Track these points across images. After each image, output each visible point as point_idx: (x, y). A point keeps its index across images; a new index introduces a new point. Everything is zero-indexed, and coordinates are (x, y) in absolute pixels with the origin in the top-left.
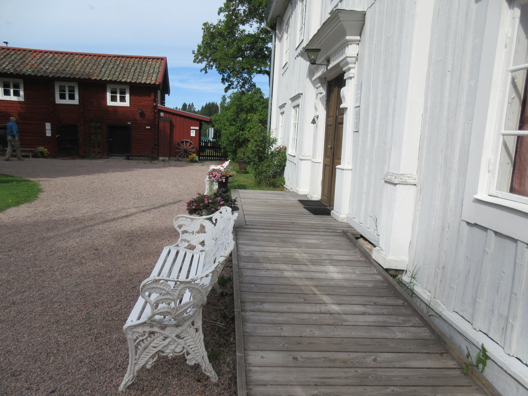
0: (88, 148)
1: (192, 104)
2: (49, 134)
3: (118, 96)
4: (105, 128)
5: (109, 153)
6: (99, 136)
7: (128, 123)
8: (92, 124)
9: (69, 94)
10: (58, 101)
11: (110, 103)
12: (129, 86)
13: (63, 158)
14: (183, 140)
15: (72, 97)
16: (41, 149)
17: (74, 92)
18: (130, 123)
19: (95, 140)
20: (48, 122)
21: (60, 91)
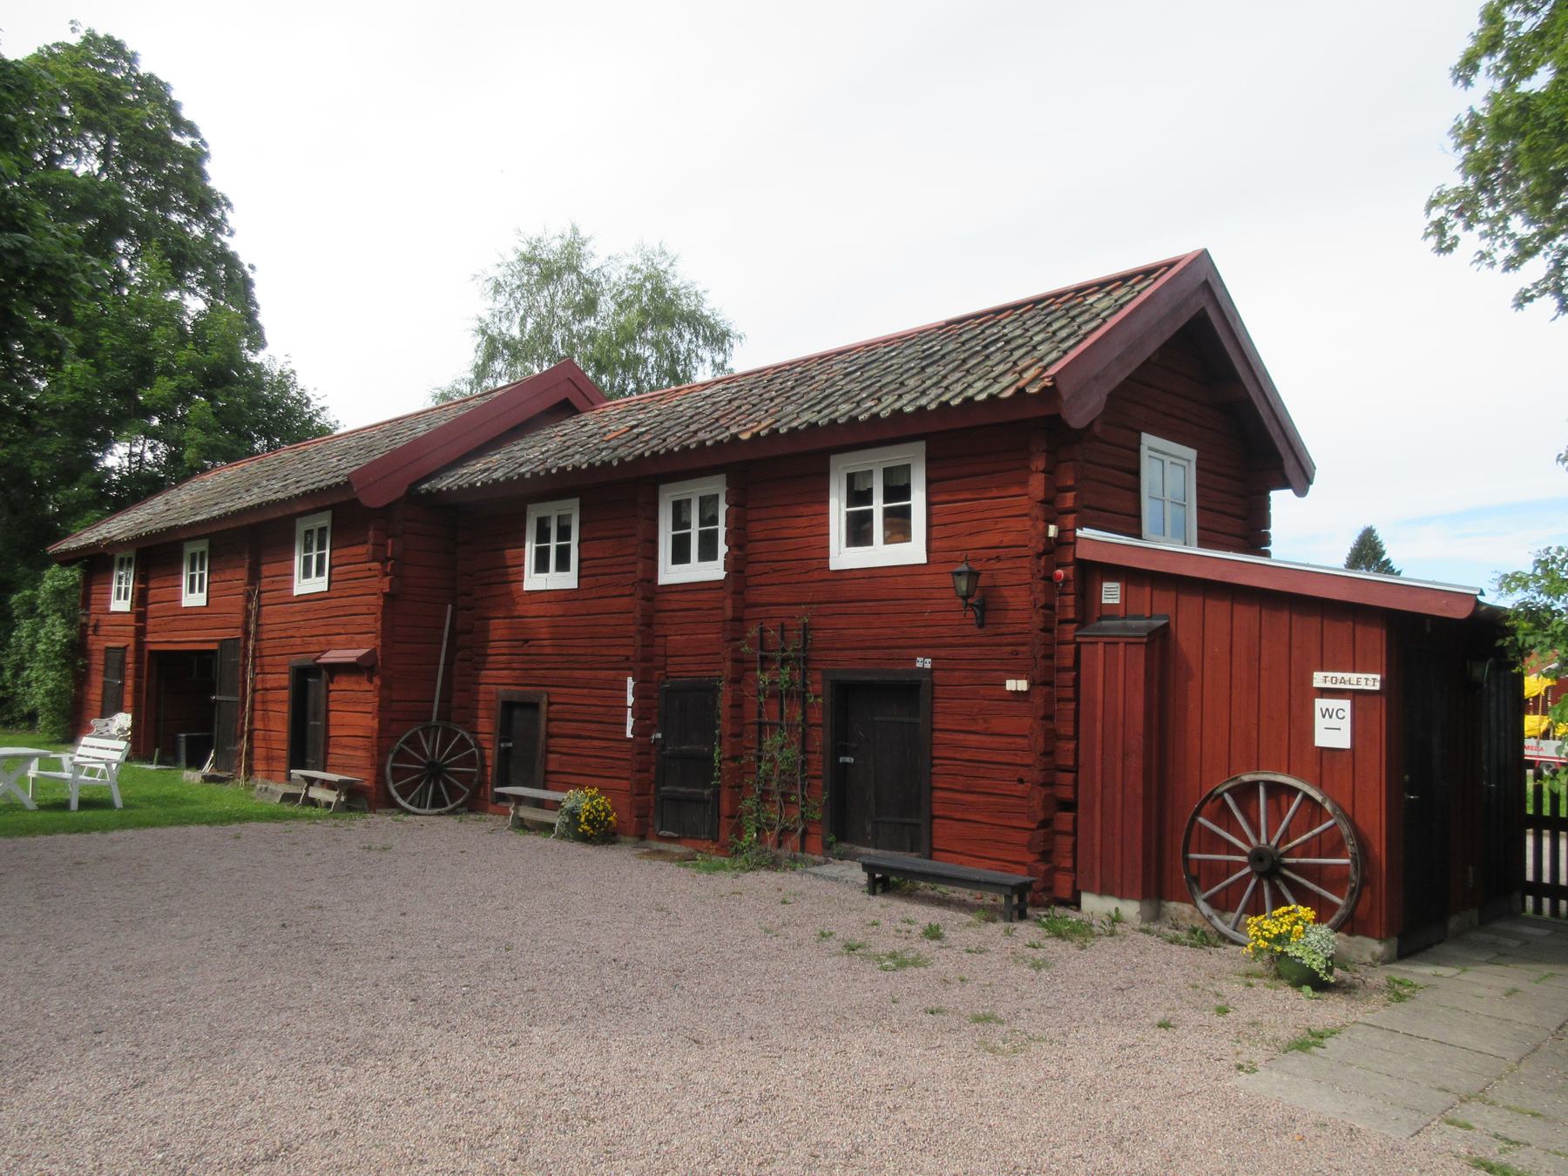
14: (1246, 778)
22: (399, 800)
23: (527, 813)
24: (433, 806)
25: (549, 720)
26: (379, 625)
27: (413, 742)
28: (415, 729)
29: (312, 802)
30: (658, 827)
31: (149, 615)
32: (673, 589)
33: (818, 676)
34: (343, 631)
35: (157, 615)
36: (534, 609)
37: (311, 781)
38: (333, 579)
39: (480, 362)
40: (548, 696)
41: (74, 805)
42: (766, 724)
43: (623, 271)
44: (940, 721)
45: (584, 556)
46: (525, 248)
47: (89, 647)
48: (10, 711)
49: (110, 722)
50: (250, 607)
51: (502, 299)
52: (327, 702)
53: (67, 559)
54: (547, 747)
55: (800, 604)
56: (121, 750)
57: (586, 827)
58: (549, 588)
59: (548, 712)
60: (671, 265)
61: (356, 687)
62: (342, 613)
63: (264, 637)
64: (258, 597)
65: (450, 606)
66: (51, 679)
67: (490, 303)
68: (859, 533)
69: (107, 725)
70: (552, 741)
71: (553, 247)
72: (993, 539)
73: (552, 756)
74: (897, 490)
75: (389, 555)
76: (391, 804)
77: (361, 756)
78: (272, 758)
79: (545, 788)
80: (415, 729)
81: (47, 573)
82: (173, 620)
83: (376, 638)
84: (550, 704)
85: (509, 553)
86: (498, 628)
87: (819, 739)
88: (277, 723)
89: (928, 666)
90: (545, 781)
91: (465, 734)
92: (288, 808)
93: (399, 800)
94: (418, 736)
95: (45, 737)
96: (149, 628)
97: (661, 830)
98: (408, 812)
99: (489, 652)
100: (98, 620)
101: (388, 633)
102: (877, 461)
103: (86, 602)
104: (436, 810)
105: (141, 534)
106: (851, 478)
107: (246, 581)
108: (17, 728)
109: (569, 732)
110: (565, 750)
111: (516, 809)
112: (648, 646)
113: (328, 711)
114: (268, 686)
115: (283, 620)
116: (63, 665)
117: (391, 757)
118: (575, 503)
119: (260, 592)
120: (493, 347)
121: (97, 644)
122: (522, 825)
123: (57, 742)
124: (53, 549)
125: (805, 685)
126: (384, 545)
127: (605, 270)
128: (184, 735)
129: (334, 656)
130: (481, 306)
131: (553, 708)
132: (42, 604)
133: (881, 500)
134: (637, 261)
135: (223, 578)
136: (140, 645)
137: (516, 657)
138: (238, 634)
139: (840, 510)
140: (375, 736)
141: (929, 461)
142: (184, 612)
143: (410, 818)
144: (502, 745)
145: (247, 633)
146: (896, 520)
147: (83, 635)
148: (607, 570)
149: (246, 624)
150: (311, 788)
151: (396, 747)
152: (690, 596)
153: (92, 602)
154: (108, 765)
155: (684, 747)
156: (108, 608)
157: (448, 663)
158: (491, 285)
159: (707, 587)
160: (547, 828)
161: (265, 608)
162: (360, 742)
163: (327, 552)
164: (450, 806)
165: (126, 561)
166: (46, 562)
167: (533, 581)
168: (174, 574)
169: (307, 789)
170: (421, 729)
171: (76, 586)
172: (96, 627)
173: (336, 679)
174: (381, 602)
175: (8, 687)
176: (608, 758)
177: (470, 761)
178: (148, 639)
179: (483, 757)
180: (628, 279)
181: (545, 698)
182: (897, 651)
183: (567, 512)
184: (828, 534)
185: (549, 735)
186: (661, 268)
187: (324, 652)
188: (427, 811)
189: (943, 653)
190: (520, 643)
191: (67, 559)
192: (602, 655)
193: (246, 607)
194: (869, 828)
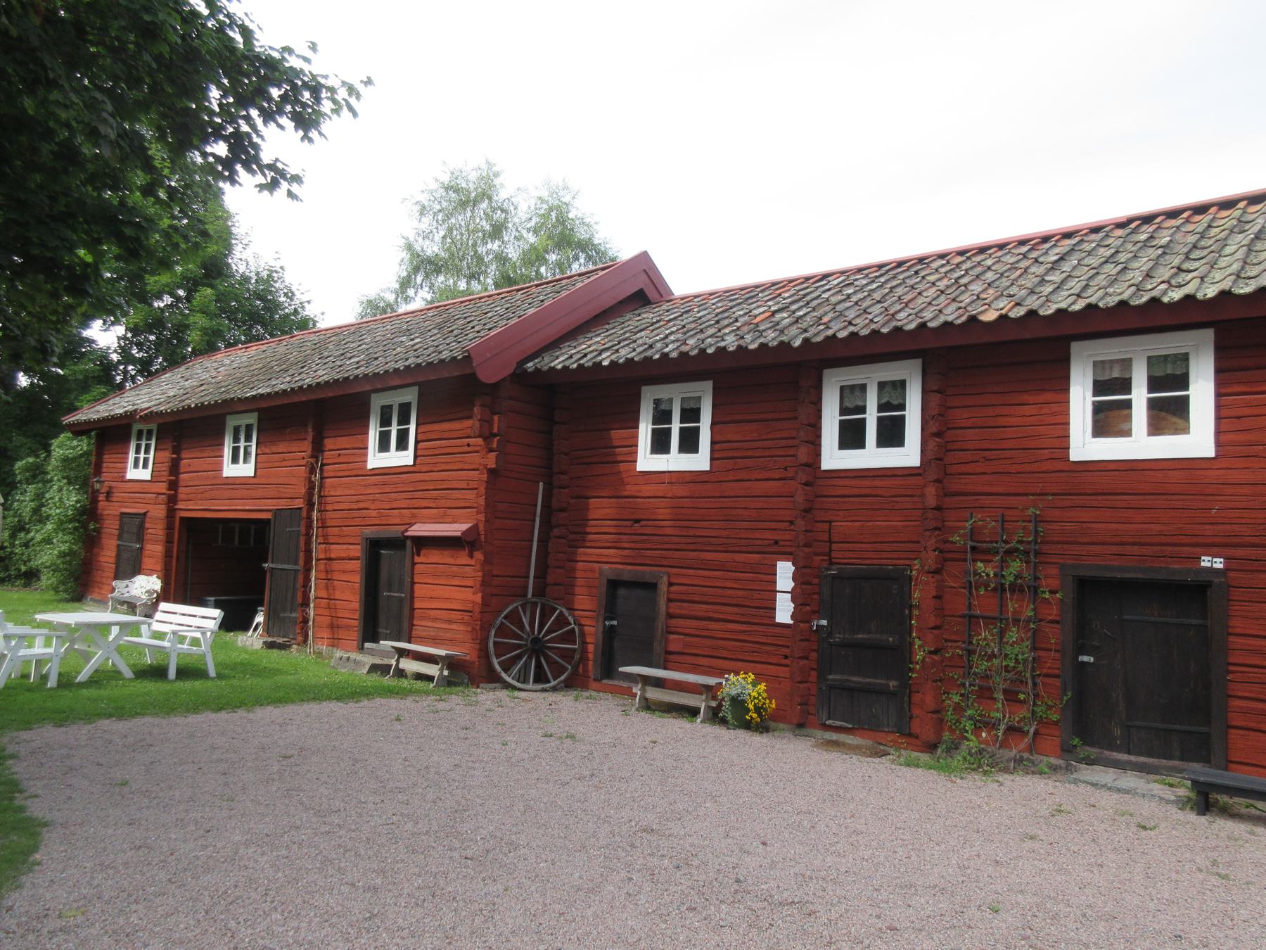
0: (956, 699)
1: (487, 162)
2: (784, 612)
3: (1140, 396)
4: (1052, 592)
5: (1076, 741)
6: (1013, 635)
7: (1206, 562)
8: (980, 564)
9: (654, 431)
10: (834, 458)
11: (376, 460)
12: (1209, 334)
13: (834, 736)
15: (689, 443)
16: (741, 684)
17: (902, 407)
18: (1219, 564)
19: (993, 656)
20: (786, 556)
21: (843, 411)
22: (504, 675)
23: (654, 694)
24: (537, 681)
25: (670, 600)
26: (482, 501)
27: (514, 617)
28: (515, 605)
29: (401, 673)
31: (181, 483)
32: (842, 475)
33: (1054, 571)
34: (434, 505)
35: (191, 484)
36: (648, 490)
37: (402, 653)
38: (418, 454)
39: (405, 274)
40: (669, 576)
41: (172, 673)
42: (977, 617)
43: (533, 202)
44: (1237, 624)
45: (717, 438)
46: (446, 178)
47: (99, 512)
48: (6, 569)
49: (130, 584)
50: (313, 479)
51: (426, 220)
52: (413, 574)
53: (80, 430)
54: (667, 627)
55: (1027, 495)
56: (215, 619)
57: (755, 716)
58: (671, 469)
59: (669, 592)
60: (574, 198)
61: (451, 561)
62: (432, 488)
63: (327, 508)
64: (321, 470)
65: (541, 484)
66: (62, 543)
67: (415, 223)
68: (852, 436)
69: (127, 586)
70: (673, 622)
71: (471, 180)
73: (672, 636)
74: (691, 414)
75: (495, 430)
76: (492, 678)
77: (459, 630)
78: (338, 627)
79: (665, 668)
80: (515, 605)
81: (55, 442)
82: (211, 490)
83: (478, 513)
84: (671, 584)
85: (617, 435)
86: (601, 509)
87: (1053, 636)
88: (350, 597)
89: (1221, 566)
90: (666, 661)
91: (564, 610)
92: (376, 679)
93: (504, 675)
94: (518, 611)
95: (50, 595)
96: (180, 496)
98: (507, 686)
99: (588, 530)
100: (110, 487)
101: (491, 509)
102: (1124, 350)
103: (98, 470)
104: (540, 686)
105: (202, 403)
106: (657, 402)
107: (309, 452)
108: (13, 585)
109: (701, 614)
110: (688, 631)
111: (643, 690)
112: (810, 531)
113: (413, 583)
114: (333, 556)
115: (353, 493)
116: (76, 529)
117: (493, 632)
118: (709, 385)
119: (323, 465)
120: (423, 266)
121: (110, 510)
122: (649, 706)
123: (68, 601)
124: (69, 419)
125: (1036, 578)
126: (490, 423)
127: (513, 199)
128: (212, 599)
129: (419, 529)
130: (408, 225)
131: (673, 588)
132: (53, 470)
133: (1144, 389)
134: (545, 194)
135: (274, 451)
136: (171, 512)
137: (625, 537)
138: (299, 503)
139: (1084, 398)
140: (477, 609)
142: (226, 482)
143: (516, 693)
144: (607, 623)
145: (310, 505)
147: (94, 501)
148: (750, 453)
149: (310, 494)
150: (401, 660)
151: (498, 622)
152: (867, 482)
153: (104, 470)
154: (204, 634)
155: (860, 636)
156: (124, 477)
157: (543, 541)
158: (418, 207)
159: (875, 474)
160: (693, 712)
161: (327, 480)
162: (458, 615)
163: (412, 427)
164: (553, 683)
165: (145, 432)
166: (59, 429)
167: (647, 461)
168: (218, 445)
169: (398, 661)
170: (521, 605)
171: (86, 454)
172: (109, 494)
173: (422, 552)
174: (485, 477)
175: (6, 547)
176: (749, 642)
177: (569, 638)
178: (181, 505)
179: (583, 634)
180: (536, 209)
181: (665, 579)
182: (1170, 548)
183: (1128, 356)
184: (1068, 424)
185: (670, 616)
186: (565, 200)
187: (411, 525)
188: (530, 686)
189: (1240, 552)
190: (629, 523)
191: (80, 430)
192: (741, 539)
193: (310, 479)
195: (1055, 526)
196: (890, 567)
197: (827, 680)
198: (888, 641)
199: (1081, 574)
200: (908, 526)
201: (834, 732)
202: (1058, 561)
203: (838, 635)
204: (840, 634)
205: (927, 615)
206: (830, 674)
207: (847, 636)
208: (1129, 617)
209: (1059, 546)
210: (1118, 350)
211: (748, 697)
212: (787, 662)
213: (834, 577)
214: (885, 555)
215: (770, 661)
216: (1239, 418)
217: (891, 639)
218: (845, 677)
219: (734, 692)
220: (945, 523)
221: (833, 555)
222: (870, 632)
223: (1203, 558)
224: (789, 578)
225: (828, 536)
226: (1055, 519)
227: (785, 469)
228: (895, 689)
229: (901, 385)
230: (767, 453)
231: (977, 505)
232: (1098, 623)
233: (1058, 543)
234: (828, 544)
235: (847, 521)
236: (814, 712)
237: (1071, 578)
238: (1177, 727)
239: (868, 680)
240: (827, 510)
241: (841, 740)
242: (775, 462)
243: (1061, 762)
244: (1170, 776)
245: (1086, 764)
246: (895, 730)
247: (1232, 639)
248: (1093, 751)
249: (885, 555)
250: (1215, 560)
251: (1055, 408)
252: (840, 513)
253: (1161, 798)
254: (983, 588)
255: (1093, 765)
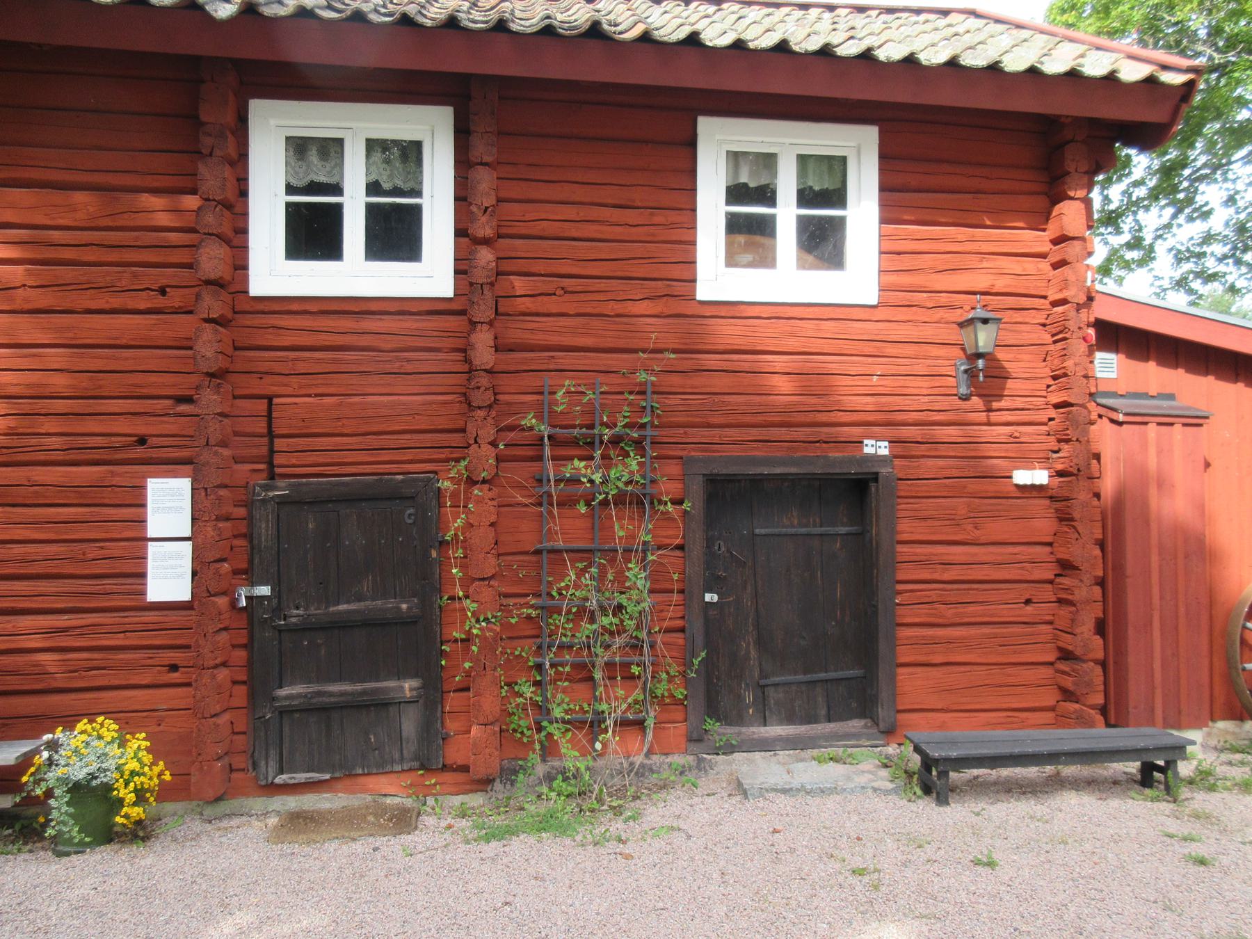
18: (883, 449)
20: (169, 465)
30: (273, 766)
44: (906, 528)
55: (635, 351)
72: (981, 281)
97: (281, 772)
109: (147, 613)
141: (885, 157)
146: (461, 203)
155: (343, 607)
194: (749, 697)
195: (674, 400)
196: (400, 477)
197: (274, 699)
198: (399, 609)
199: (715, 471)
200: (431, 403)
201: (288, 794)
202: (680, 453)
203: (295, 612)
204: (297, 608)
205: (482, 556)
206: (281, 687)
207: (312, 611)
208: (763, 531)
209: (681, 431)
210: (760, 139)
211: (116, 775)
212: (175, 677)
213: (282, 502)
214: (385, 456)
215: (135, 680)
216: (899, 253)
217: (404, 606)
218: (313, 688)
219: (79, 774)
220: (500, 397)
221: (279, 459)
222: (360, 598)
223: (866, 442)
224: (179, 510)
225: (264, 424)
226: (673, 390)
227: (163, 291)
228: (414, 693)
229: (411, 152)
230: (114, 256)
231: (552, 367)
232: (722, 543)
233: (679, 425)
234: (266, 439)
235: (310, 396)
236: (242, 766)
237: (701, 478)
238: (822, 675)
239: (359, 687)
240: (262, 374)
241: (306, 807)
242: (135, 275)
243: (689, 760)
244: (831, 746)
245: (723, 754)
246: (416, 764)
247: (900, 548)
248: (733, 732)
249: (385, 456)
250: (879, 443)
251: (673, 217)
252: (294, 379)
253: (875, 790)
254: (582, 503)
255: (733, 752)
